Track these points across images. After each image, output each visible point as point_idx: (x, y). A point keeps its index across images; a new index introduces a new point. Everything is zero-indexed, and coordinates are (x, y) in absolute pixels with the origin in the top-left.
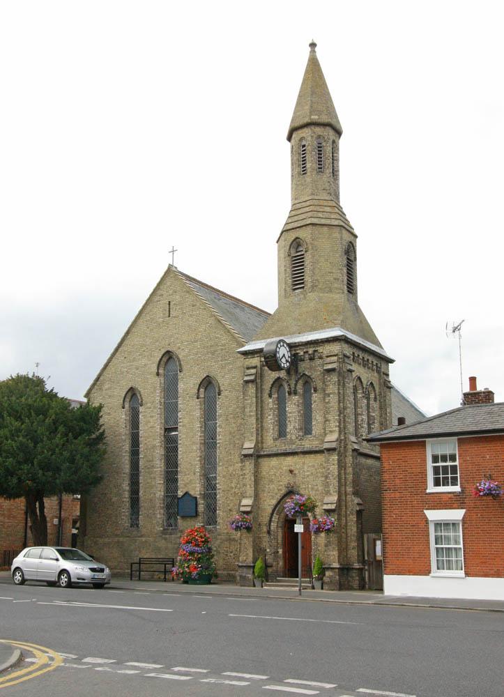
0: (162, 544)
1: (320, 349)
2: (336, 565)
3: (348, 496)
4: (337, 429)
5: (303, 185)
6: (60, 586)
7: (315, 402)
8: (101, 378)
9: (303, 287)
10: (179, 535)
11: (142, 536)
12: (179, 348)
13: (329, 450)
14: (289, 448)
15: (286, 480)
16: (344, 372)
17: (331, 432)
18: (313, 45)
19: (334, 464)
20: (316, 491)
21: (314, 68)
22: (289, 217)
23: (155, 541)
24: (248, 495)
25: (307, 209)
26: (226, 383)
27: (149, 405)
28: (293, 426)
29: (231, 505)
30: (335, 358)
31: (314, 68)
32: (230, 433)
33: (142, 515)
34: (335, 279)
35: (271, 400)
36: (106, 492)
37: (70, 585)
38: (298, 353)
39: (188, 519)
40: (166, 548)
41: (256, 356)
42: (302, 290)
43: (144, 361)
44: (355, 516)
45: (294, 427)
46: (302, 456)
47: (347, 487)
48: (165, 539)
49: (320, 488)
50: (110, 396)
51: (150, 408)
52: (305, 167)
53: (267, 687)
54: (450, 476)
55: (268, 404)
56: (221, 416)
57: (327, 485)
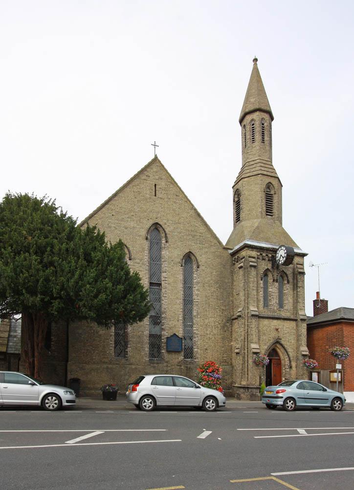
6: (206, 410)
9: (272, 216)
10: (165, 364)
11: (131, 364)
12: (166, 224)
14: (270, 314)
15: (274, 334)
18: (255, 60)
21: (256, 77)
24: (254, 342)
28: (274, 301)
31: (256, 77)
32: (206, 297)
33: (130, 347)
35: (262, 282)
37: (156, 408)
39: (173, 353)
45: (276, 302)
46: (282, 321)
48: (154, 367)
49: (293, 341)
51: (139, 263)
52: (254, 138)
55: (260, 284)
56: (198, 283)
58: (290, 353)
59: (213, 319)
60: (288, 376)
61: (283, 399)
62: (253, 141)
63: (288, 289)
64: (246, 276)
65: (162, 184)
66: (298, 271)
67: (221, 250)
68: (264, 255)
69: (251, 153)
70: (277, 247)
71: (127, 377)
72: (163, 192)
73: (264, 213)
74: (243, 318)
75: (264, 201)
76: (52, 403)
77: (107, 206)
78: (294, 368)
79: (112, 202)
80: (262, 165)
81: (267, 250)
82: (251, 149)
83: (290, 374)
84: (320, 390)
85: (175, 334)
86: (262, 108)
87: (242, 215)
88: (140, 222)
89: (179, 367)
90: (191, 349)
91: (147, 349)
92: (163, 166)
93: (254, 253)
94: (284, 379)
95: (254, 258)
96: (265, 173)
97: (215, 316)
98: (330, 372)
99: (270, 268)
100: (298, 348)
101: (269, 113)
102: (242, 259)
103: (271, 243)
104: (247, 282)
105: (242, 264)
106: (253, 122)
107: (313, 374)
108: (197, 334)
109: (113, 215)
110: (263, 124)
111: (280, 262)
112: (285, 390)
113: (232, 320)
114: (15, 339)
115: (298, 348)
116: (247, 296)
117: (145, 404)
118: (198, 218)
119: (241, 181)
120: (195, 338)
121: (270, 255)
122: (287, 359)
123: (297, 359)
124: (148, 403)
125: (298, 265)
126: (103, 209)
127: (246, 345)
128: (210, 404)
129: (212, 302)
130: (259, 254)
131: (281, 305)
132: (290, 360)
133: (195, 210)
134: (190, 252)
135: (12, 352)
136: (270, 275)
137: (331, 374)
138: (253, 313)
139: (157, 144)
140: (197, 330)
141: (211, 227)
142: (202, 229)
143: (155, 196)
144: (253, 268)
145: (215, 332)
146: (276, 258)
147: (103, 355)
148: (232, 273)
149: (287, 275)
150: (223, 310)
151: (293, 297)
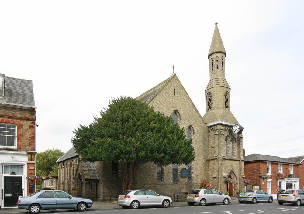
0: (174, 187)
1: (214, 128)
14: (228, 158)
15: (230, 167)
21: (217, 33)
22: (210, 81)
23: (171, 186)
29: (198, 174)
31: (217, 33)
37: (140, 207)
40: (176, 189)
48: (175, 185)
54: (2, 128)
60: (236, 188)
61: (252, 198)
62: (217, 68)
63: (236, 145)
64: (219, 139)
65: (178, 89)
66: (240, 136)
67: (203, 124)
68: (226, 128)
69: (217, 74)
70: (234, 125)
71: (164, 191)
72: (178, 93)
73: (225, 106)
74: (218, 160)
76: (166, 204)
77: (153, 100)
78: (238, 184)
80: (223, 81)
81: (228, 126)
82: (217, 72)
83: (237, 187)
84: (155, 195)
85: (185, 168)
86: (223, 51)
87: (212, 106)
91: (172, 176)
92: (178, 79)
93: (222, 128)
94: (234, 189)
95: (222, 130)
96: (225, 86)
98: (253, 185)
99: (228, 135)
100: (240, 174)
101: (225, 54)
102: (216, 130)
103: (229, 122)
104: (220, 142)
105: (217, 133)
106: (217, 58)
108: (194, 168)
110: (222, 60)
111: (235, 133)
112: (72, 198)
113: (208, 160)
114: (92, 171)
115: (240, 174)
116: (220, 149)
117: (202, 203)
118: (193, 107)
119: (212, 89)
120: (193, 170)
121: (229, 129)
122: (235, 180)
123: (240, 179)
124: (203, 202)
125: (221, 130)
126: (152, 102)
127: (219, 173)
128: (166, 204)
129: (200, 151)
130: (224, 128)
131: (233, 153)
132: (237, 180)
133: (193, 103)
134: (191, 125)
135: (93, 179)
136: (228, 138)
137: (253, 186)
138: (223, 157)
139: (174, 67)
140: (193, 166)
141: (199, 112)
142: (195, 113)
143: (175, 95)
144: (222, 135)
145: (201, 166)
146: (232, 130)
147: (152, 180)
148: (209, 136)
149: (235, 138)
150: (205, 155)
151: (238, 149)
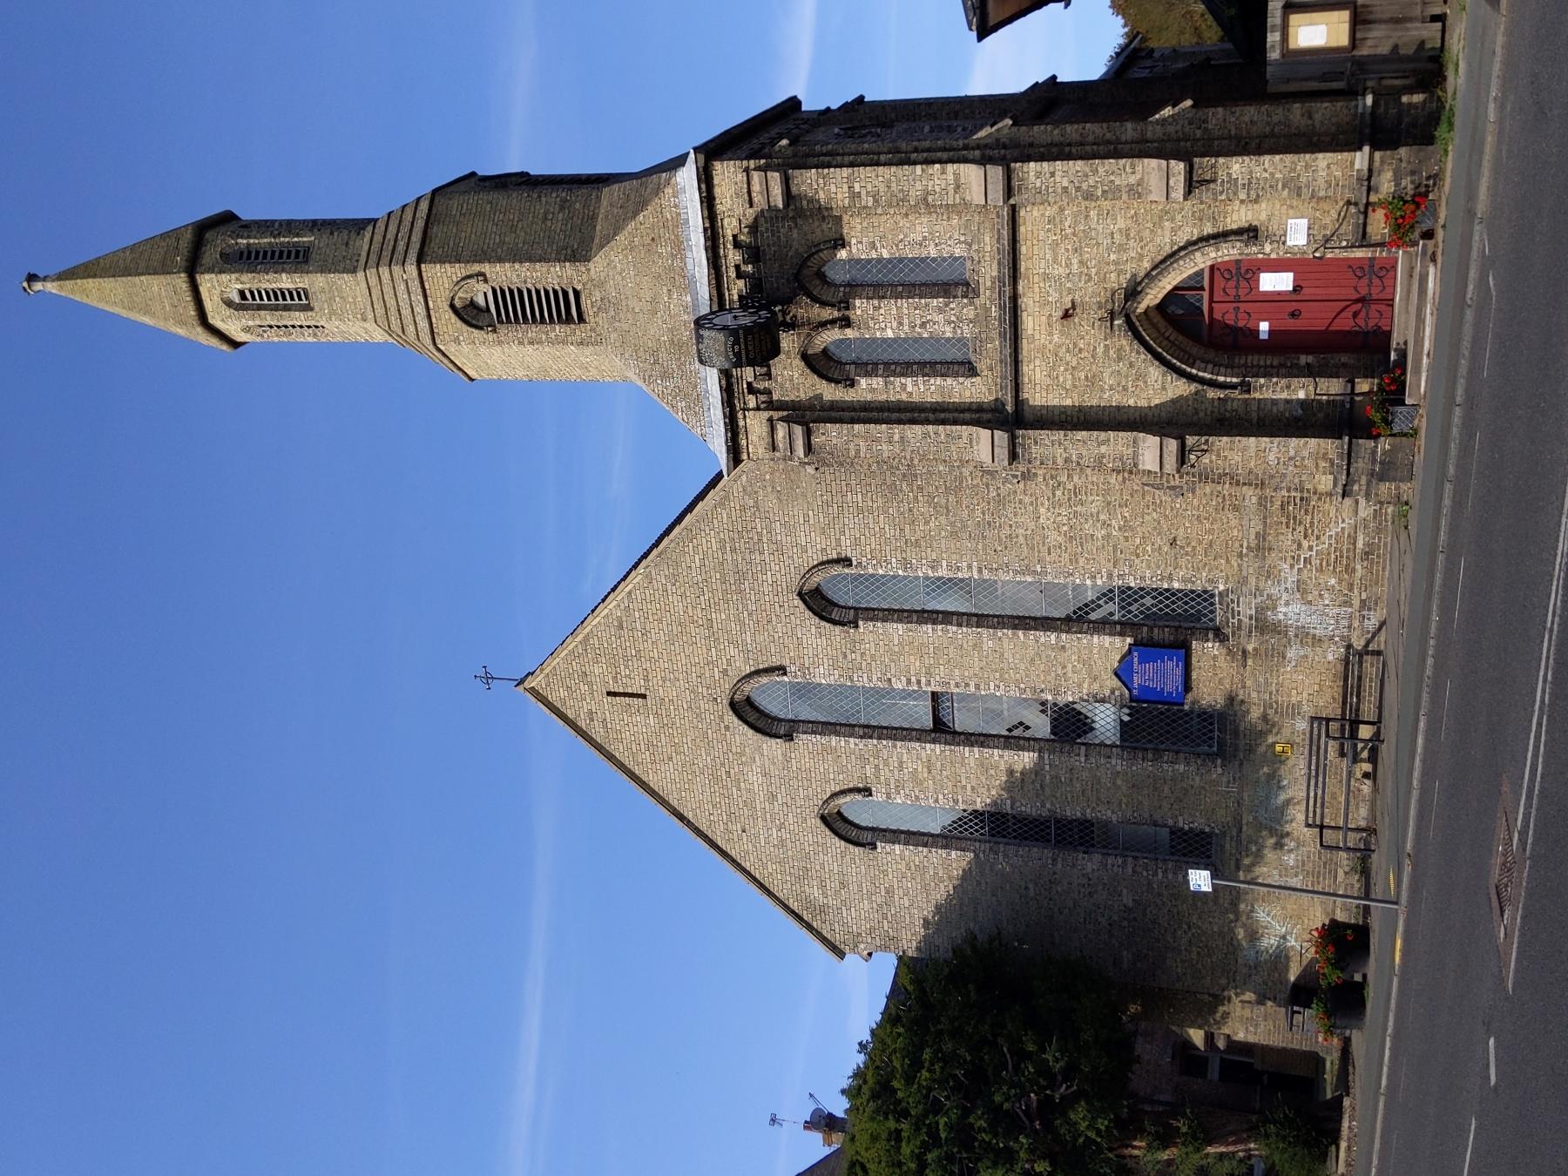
2: (1360, 159)
3: (1149, 135)
4: (950, 168)
5: (332, 299)
7: (873, 246)
8: (795, 906)
9: (577, 294)
13: (1009, 192)
15: (1089, 331)
16: (795, 155)
17: (958, 187)
19: (1053, 174)
20: (1128, 236)
24: (1130, 451)
25: (388, 289)
26: (819, 541)
27: (869, 770)
30: (756, 176)
34: (562, 208)
36: (1103, 921)
38: (740, 297)
41: (741, 423)
42: (583, 298)
43: (755, 778)
44: (1211, 111)
45: (940, 310)
47: (1123, 138)
49: (1121, 224)
50: (843, 885)
51: (877, 766)
52: (291, 294)
53: (1510, 986)
57: (1112, 193)
58: (1182, 238)
59: (1042, 510)
73: (580, 331)
75: (533, 331)
79: (704, 828)
88: (742, 754)
89: (1250, 662)
90: (1175, 832)
97: (1027, 500)
107: (1290, 276)
109: (744, 831)
126: (733, 853)
